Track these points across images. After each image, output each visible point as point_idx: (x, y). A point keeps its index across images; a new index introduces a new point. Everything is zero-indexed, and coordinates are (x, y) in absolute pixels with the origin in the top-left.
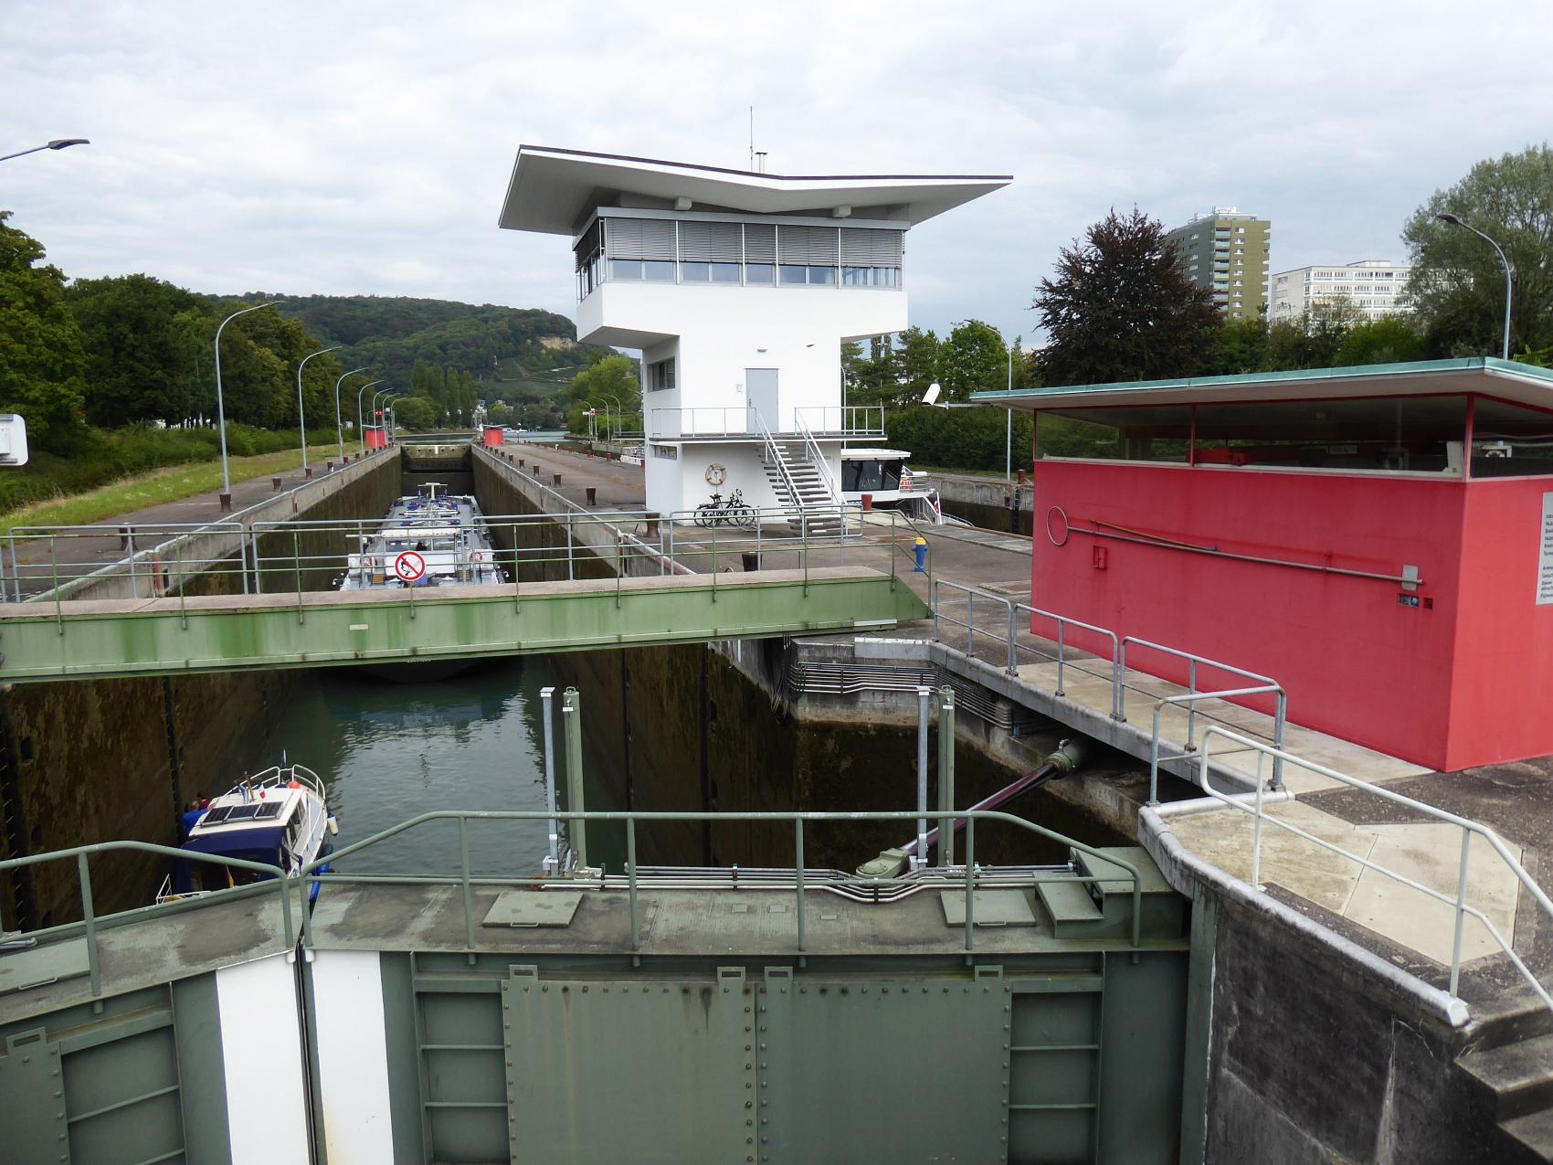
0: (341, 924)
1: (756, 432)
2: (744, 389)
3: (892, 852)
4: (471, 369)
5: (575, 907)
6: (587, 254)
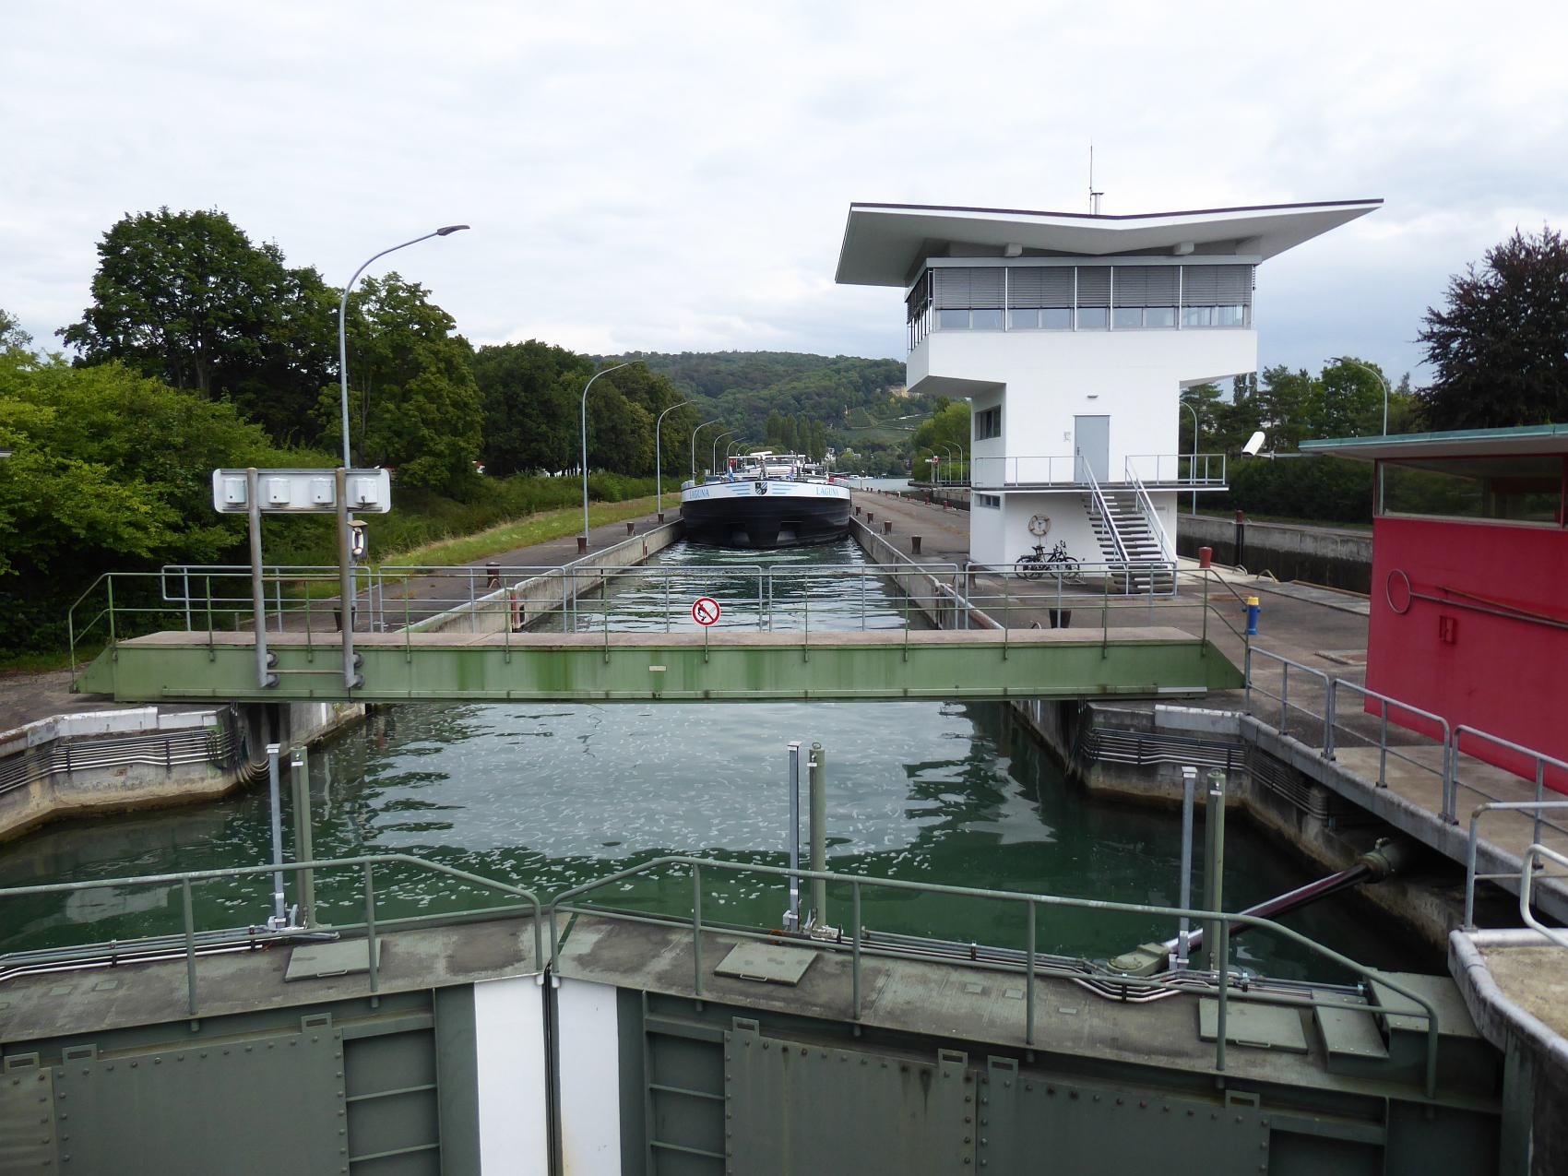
0: (589, 955)
1: (1082, 481)
2: (1072, 437)
3: (1151, 947)
4: (821, 418)
5: (807, 966)
6: (916, 307)
